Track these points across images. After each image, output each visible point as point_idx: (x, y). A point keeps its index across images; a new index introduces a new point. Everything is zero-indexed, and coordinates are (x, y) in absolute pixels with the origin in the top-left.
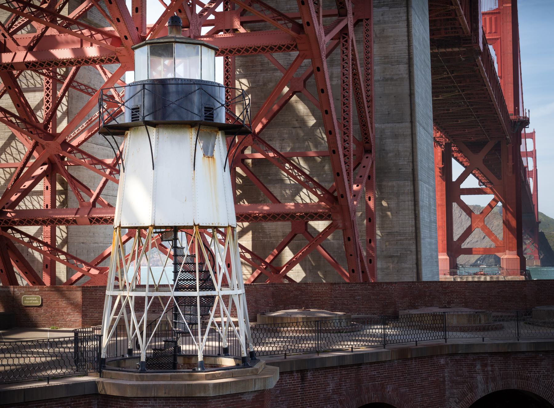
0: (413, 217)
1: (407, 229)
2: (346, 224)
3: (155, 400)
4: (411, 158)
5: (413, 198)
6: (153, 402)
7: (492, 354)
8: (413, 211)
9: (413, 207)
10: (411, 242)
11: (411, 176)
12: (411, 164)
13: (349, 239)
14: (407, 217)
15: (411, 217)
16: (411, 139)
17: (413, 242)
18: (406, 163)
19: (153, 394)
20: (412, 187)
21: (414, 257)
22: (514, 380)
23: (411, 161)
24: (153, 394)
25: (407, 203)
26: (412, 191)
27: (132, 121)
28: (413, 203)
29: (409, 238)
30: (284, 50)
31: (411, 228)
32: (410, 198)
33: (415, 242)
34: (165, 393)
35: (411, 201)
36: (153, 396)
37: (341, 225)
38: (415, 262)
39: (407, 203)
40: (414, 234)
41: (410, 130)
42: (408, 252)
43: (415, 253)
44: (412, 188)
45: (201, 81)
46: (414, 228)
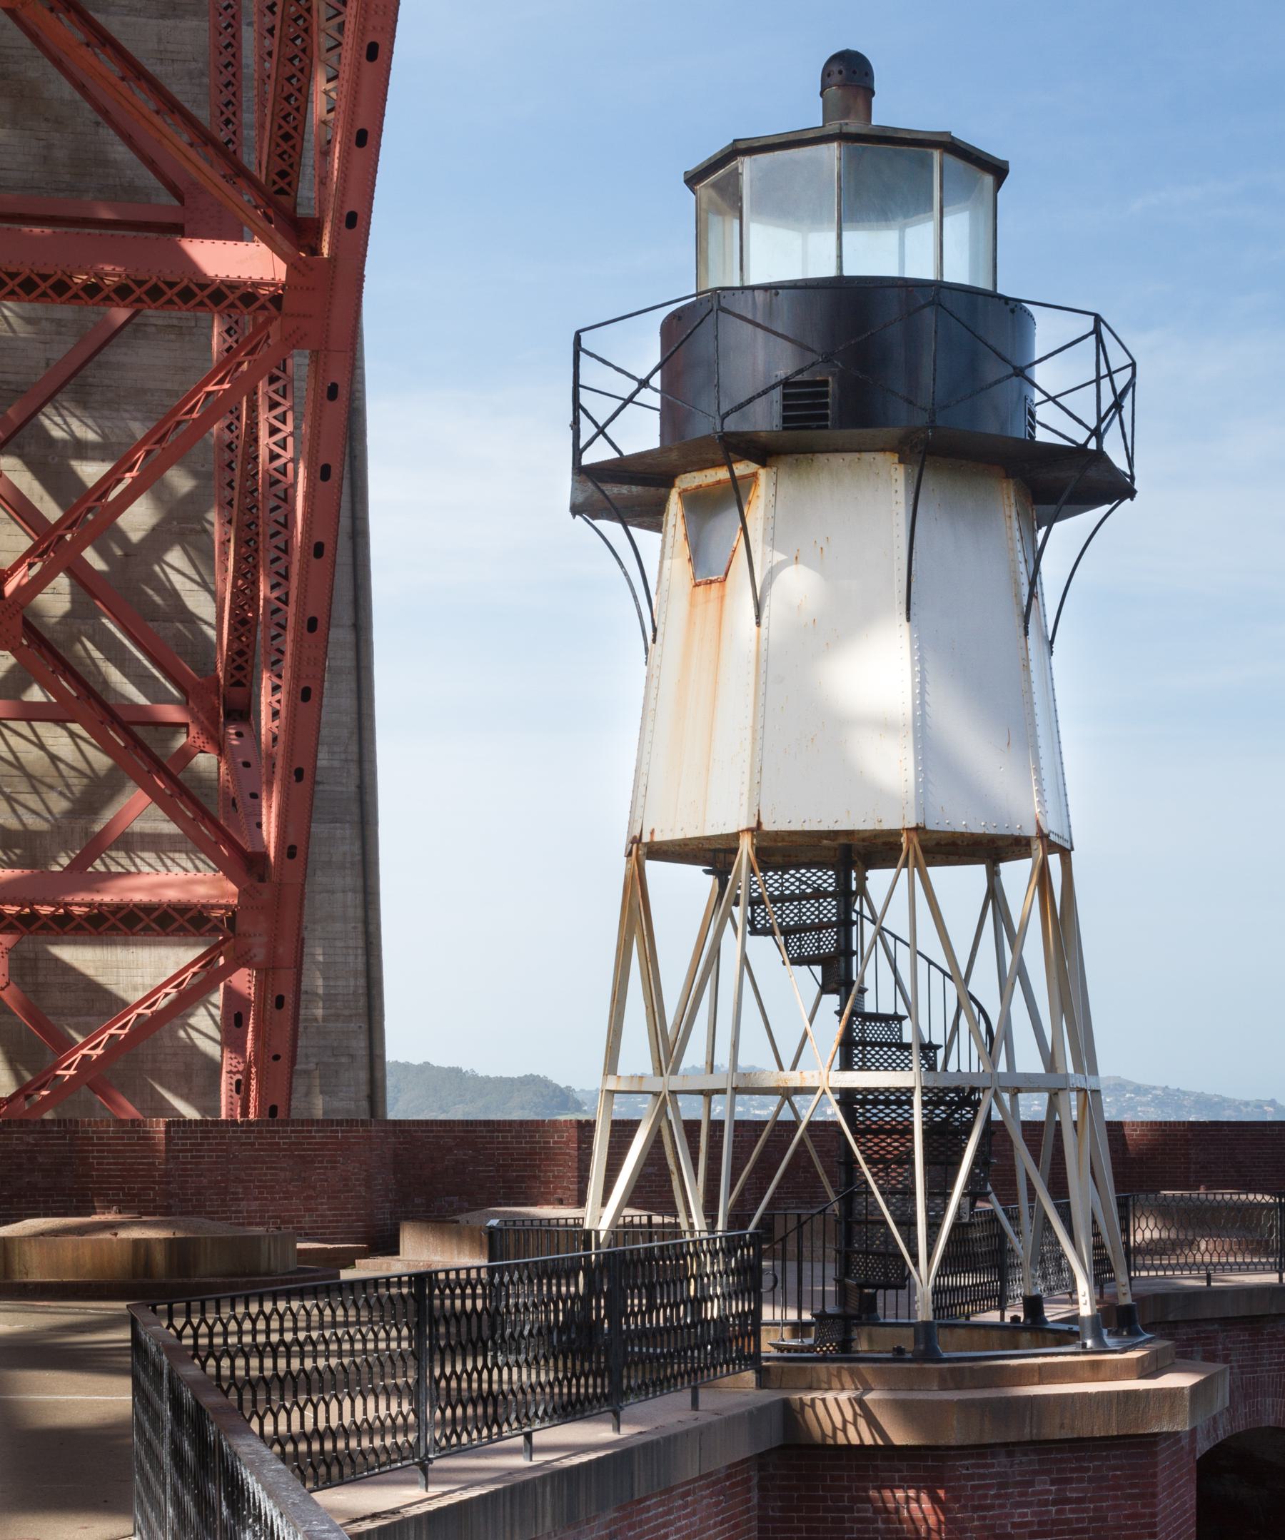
0: (361, 943)
1: (341, 983)
2: (281, 950)
3: (1010, 1454)
4: (354, 748)
5: (359, 883)
6: (1004, 1460)
7: (1227, 1322)
8: (360, 926)
9: (360, 913)
10: (353, 1026)
11: (354, 808)
12: (354, 769)
13: (280, 1002)
14: (339, 944)
15: (351, 943)
16: (353, 685)
17: (359, 1025)
18: (336, 764)
19: (1027, 1430)
20: (357, 844)
21: (363, 1075)
22: (1269, 1401)
23: (355, 757)
24: (1027, 1430)
25: (339, 896)
26: (358, 858)
27: (785, 429)
28: (360, 897)
29: (347, 1012)
30: (44, 294)
31: (352, 983)
32: (349, 881)
33: (365, 1026)
34: (1062, 1426)
35: (354, 891)
36: (1027, 1438)
37: (260, 954)
38: (364, 1090)
39: (339, 896)
40: (362, 1002)
41: (350, 654)
42: (344, 1060)
43: (365, 1060)
44: (356, 848)
45: (993, 295)
46: (362, 982)
